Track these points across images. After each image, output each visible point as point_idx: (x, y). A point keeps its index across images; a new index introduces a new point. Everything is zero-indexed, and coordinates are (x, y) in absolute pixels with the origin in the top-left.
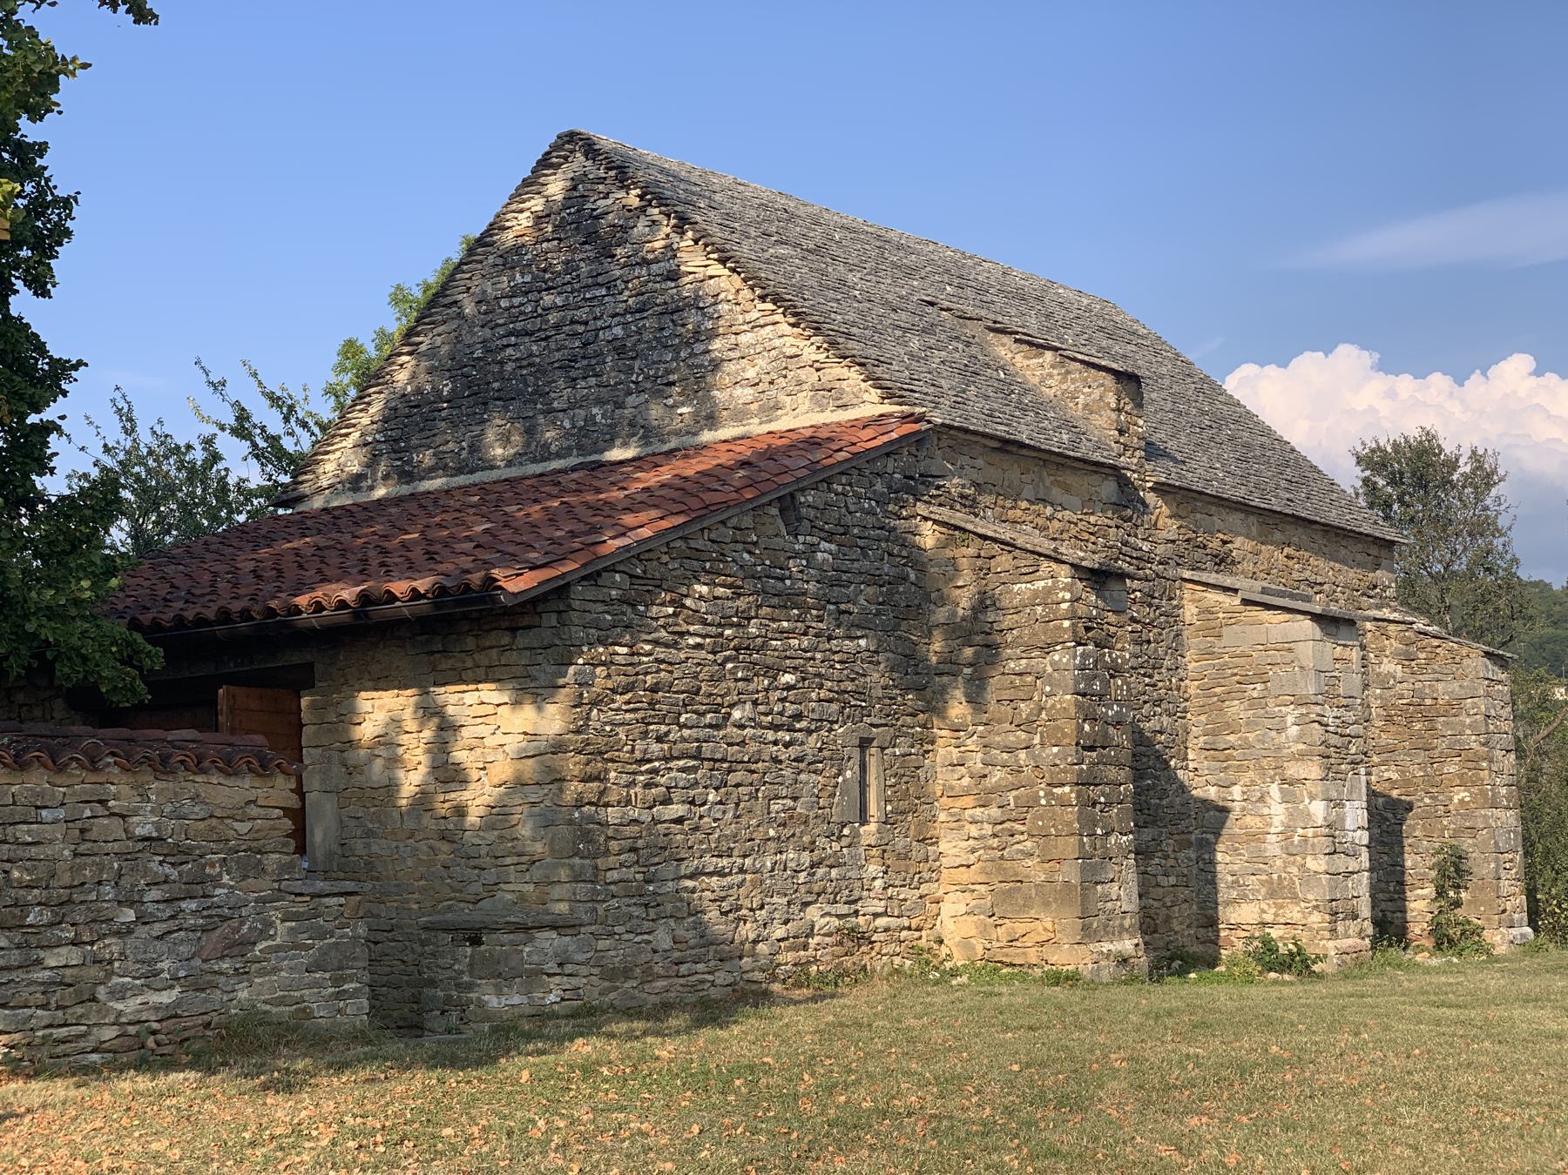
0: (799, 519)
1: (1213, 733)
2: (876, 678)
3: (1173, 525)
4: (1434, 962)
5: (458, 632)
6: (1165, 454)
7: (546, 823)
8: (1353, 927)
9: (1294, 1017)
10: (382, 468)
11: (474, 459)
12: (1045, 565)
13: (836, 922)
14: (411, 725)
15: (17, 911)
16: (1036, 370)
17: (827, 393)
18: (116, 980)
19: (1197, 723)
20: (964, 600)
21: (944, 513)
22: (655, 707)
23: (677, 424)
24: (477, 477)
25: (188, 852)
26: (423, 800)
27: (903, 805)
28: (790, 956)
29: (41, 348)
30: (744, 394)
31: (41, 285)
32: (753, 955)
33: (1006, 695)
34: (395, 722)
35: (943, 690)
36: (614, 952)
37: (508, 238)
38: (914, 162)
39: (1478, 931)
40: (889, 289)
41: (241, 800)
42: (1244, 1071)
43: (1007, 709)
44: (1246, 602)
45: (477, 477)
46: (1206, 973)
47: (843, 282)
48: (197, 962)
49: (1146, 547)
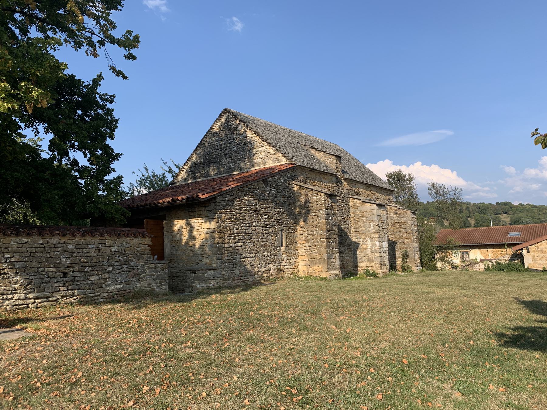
0: (268, 184)
1: (356, 228)
2: (284, 217)
3: (348, 186)
4: (402, 274)
5: (192, 207)
6: (346, 172)
7: (212, 247)
8: (385, 267)
9: (370, 288)
10: (190, 177)
11: (208, 175)
12: (319, 193)
13: (276, 267)
14: (185, 227)
15: (82, 268)
16: (320, 156)
17: (275, 159)
18: (107, 283)
19: (353, 226)
20: (303, 201)
21: (299, 183)
22: (236, 222)
23: (247, 167)
24: (208, 178)
25: (125, 254)
26: (187, 243)
27: (290, 243)
28: (266, 275)
29: (112, 150)
30: (260, 160)
31: (112, 138)
32: (258, 274)
33: (311, 220)
34: (182, 227)
35: (299, 219)
36: (226, 274)
37: (214, 130)
38: (293, 114)
39: (411, 268)
40: (290, 140)
41: (141, 243)
42: (357, 303)
43: (312, 223)
44: (363, 202)
45: (208, 178)
46: (355, 277)
47: (280, 138)
48: (127, 278)
49: (342, 191)
